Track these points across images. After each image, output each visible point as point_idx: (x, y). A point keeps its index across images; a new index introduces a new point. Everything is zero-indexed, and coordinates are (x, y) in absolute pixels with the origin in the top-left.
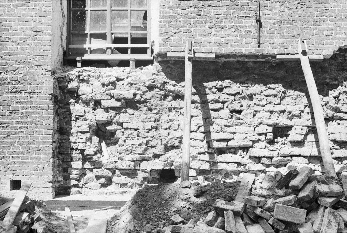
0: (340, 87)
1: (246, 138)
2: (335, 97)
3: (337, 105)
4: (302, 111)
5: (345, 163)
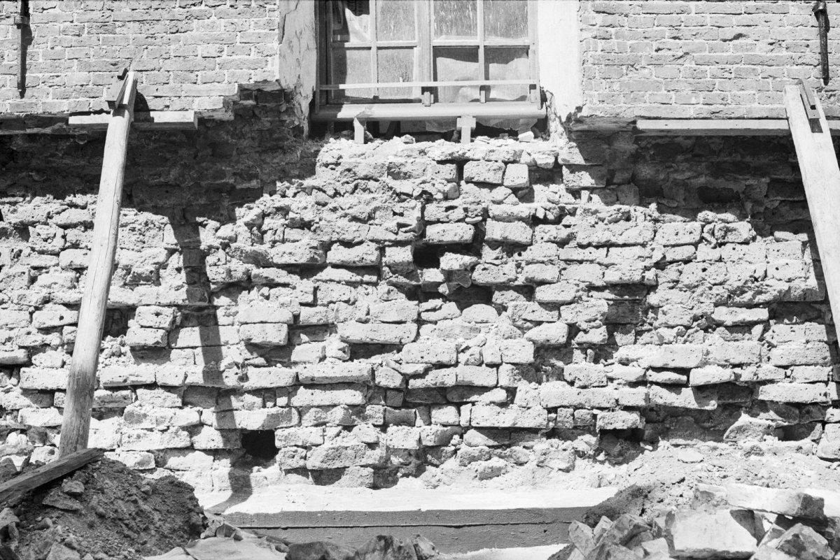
0: (266, 197)
1: (9, 339)
4: (163, 266)
5: (284, 404)
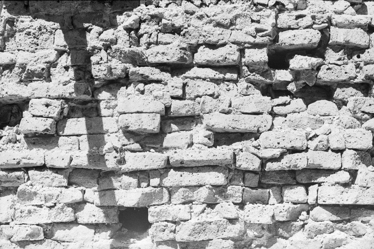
0: (143, 6)
2: (128, 30)
3: (134, 48)
4: (53, 64)
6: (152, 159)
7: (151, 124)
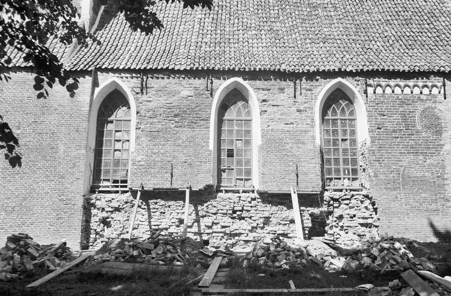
6: (210, 231)
7: (210, 224)
